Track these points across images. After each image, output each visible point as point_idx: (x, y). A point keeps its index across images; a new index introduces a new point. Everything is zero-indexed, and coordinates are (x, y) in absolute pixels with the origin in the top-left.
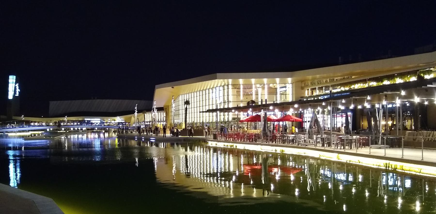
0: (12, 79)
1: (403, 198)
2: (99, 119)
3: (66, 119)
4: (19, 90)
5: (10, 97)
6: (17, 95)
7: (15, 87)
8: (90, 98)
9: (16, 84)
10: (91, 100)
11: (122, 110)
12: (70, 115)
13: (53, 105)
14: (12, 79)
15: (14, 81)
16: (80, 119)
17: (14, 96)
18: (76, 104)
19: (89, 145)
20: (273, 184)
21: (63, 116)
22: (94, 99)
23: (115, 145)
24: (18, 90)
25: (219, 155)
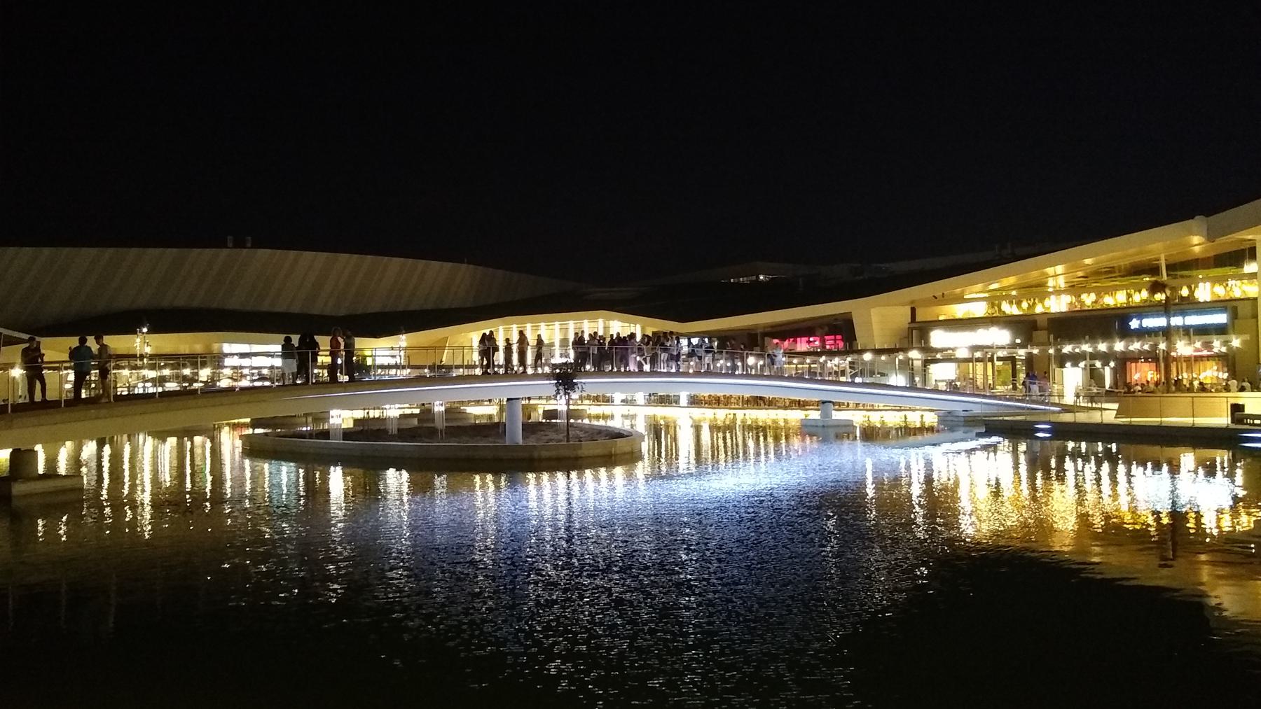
10: (224, 253)
11: (375, 307)
22: (239, 244)
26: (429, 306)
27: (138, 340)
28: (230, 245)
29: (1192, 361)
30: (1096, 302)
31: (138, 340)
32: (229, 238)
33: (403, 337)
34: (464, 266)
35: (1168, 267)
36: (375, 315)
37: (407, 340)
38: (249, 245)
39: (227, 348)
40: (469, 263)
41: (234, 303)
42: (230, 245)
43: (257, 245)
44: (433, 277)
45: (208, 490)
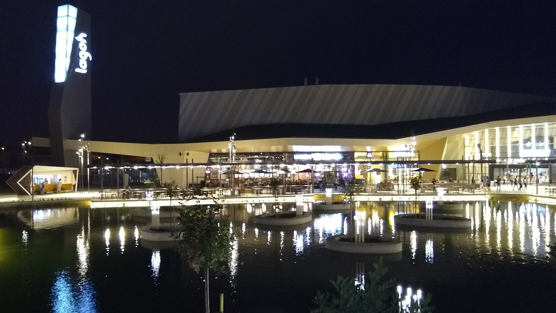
0: (67, 17)
1: (104, 166)
2: (338, 148)
3: (230, 146)
4: (89, 55)
5: (60, 76)
6: (83, 69)
7: (76, 44)
8: (300, 83)
9: (77, 32)
10: (302, 88)
11: (397, 119)
12: (245, 133)
13: (193, 104)
14: (67, 17)
15: (73, 23)
16: (274, 149)
17: (71, 73)
18: (260, 101)
19: (147, 210)
20: (423, 290)
21: (223, 136)
22: (311, 83)
23: (475, 242)
24: (85, 55)
25: (495, 211)
26: (434, 116)
27: (230, 144)
28: (306, 83)
29: (319, 210)
30: (500, 163)
31: (230, 144)
32: (306, 79)
33: (414, 138)
34: (459, 88)
35: (101, 185)
36: (397, 123)
37: (416, 140)
38: (317, 83)
39: (295, 148)
40: (463, 85)
41: (307, 120)
42: (306, 83)
43: (323, 82)
44: (437, 96)
45: (381, 231)
